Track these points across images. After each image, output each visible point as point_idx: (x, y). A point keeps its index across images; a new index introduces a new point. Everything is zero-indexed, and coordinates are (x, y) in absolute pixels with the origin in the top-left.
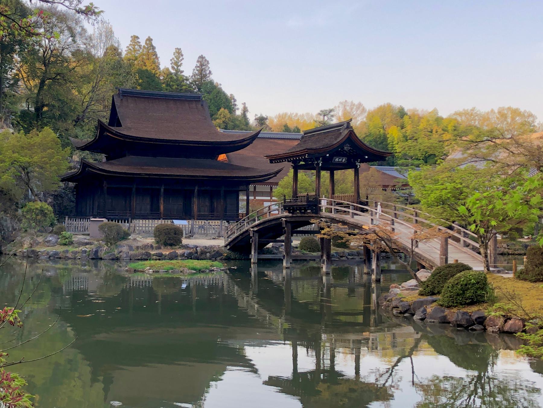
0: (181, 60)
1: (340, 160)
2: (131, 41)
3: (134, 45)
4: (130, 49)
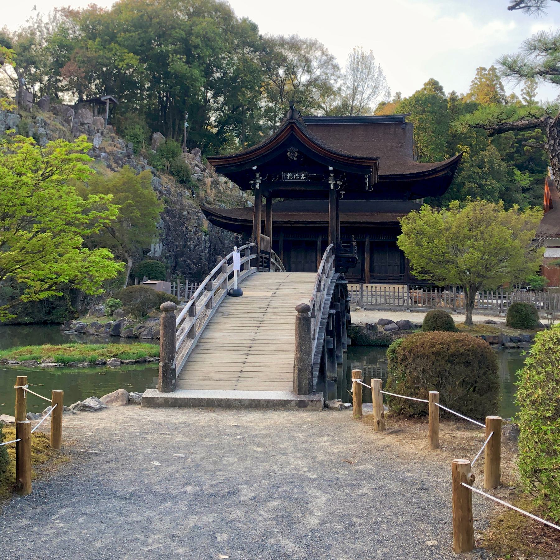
0: (535, 89)
1: (296, 176)
2: (477, 74)
3: (480, 78)
4: (476, 84)
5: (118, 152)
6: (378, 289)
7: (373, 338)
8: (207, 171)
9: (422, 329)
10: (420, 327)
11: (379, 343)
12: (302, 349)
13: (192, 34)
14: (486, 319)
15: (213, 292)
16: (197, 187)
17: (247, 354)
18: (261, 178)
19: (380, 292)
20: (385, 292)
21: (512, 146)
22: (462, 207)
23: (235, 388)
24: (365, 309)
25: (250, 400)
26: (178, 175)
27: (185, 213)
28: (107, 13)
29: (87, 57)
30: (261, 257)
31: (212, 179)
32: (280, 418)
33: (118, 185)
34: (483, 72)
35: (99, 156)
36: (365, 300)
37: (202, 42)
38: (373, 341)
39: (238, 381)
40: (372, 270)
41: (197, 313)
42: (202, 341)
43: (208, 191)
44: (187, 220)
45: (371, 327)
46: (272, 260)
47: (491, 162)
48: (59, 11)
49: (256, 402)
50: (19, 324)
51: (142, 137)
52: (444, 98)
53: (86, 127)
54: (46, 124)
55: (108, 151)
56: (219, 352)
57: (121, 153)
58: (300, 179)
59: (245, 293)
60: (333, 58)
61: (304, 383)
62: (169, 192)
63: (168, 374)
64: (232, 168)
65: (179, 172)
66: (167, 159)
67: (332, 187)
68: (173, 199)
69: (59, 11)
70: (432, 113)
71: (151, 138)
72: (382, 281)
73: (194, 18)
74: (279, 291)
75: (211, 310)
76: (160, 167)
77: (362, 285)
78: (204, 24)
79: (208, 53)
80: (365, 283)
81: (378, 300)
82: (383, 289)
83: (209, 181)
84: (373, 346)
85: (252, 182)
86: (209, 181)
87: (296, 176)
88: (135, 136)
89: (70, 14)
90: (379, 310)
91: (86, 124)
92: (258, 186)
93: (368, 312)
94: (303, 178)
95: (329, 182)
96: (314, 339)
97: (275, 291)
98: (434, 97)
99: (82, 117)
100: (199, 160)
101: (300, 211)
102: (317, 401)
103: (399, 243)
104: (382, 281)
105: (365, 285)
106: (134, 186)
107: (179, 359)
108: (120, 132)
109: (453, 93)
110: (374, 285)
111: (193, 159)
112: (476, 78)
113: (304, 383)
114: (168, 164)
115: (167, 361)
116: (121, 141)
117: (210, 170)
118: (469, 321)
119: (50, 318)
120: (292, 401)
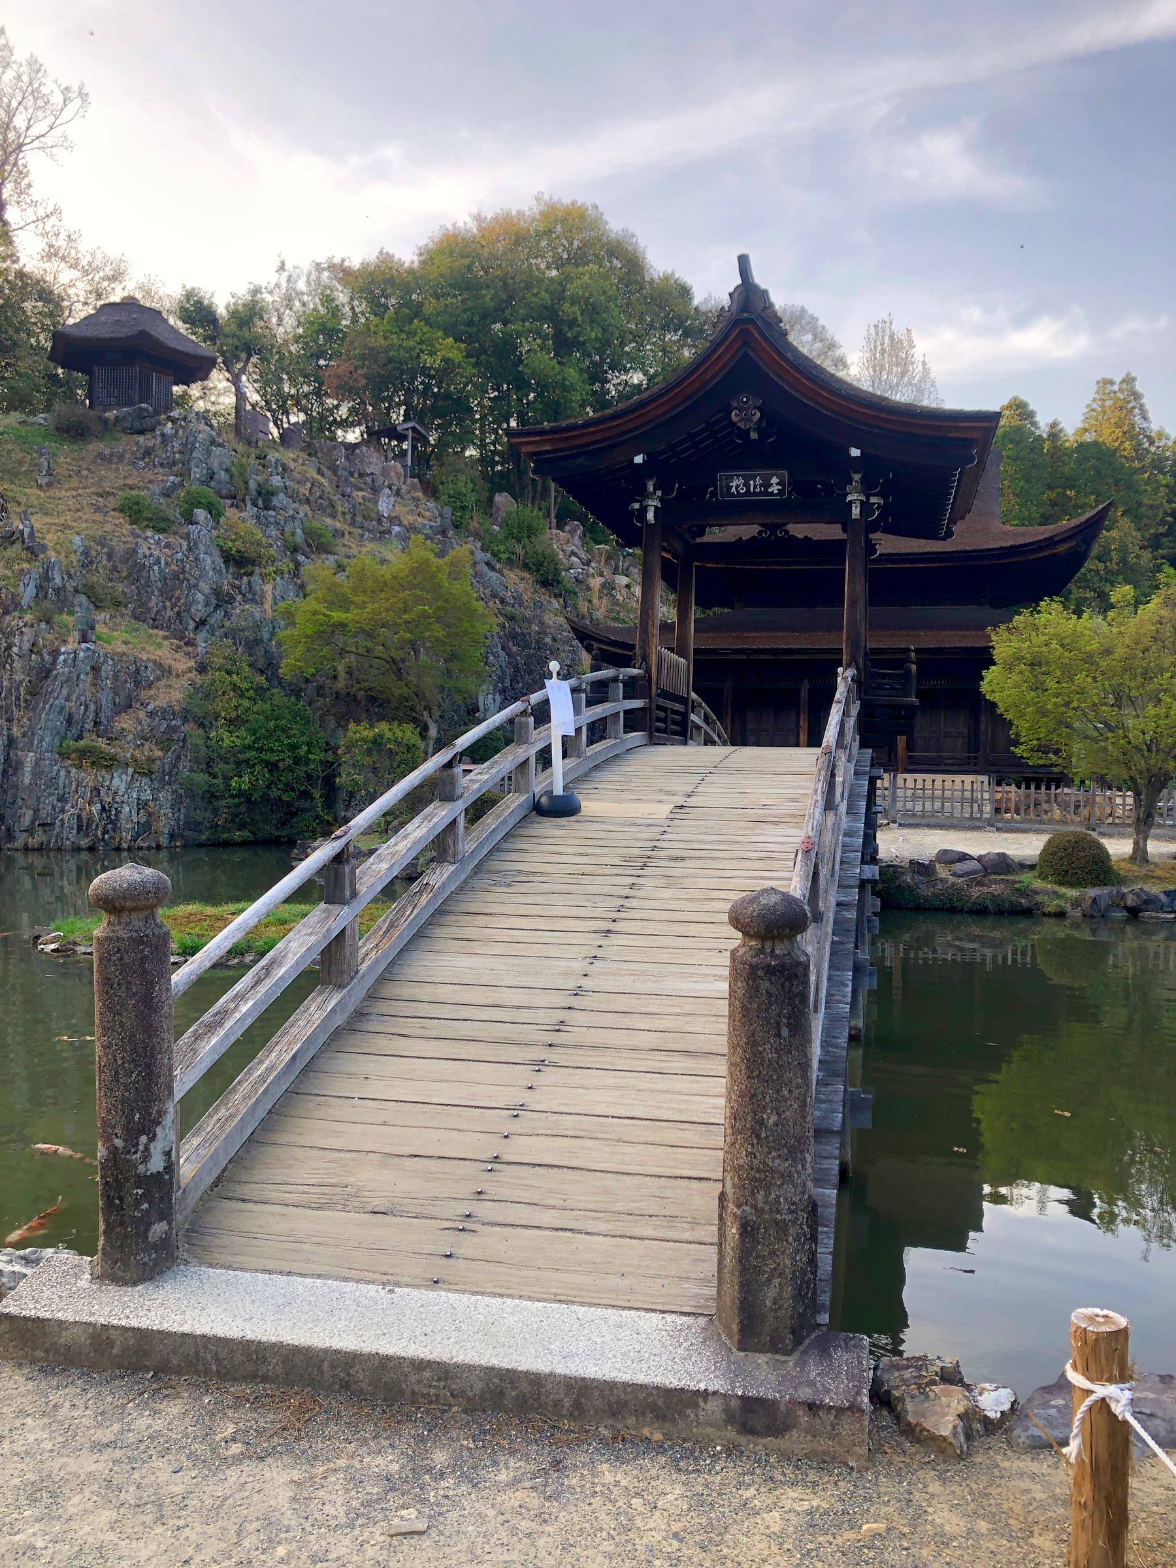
1: (755, 484)
2: (1097, 392)
4: (1093, 410)
5: (424, 525)
6: (929, 784)
7: (926, 891)
8: (593, 564)
9: (1036, 873)
10: (1032, 867)
11: (938, 904)
12: (762, 1123)
13: (564, 299)
15: (460, 806)
16: (575, 594)
17: (540, 1065)
18: (659, 493)
19: (933, 789)
20: (943, 790)
21: (1163, 522)
22: (1139, 601)
23: (441, 1268)
24: (900, 825)
25: (490, 1370)
26: (538, 571)
27: (548, 640)
28: (411, 271)
29: (369, 348)
30: (660, 708)
31: (602, 580)
32: (642, 1502)
33: (401, 575)
34: (1109, 388)
35: (389, 532)
36: (899, 805)
37: (582, 314)
38: (926, 899)
39: (465, 1225)
41: (362, 888)
42: (391, 990)
43: (595, 601)
44: (552, 653)
45: (921, 868)
46: (693, 717)
47: (1123, 550)
48: (323, 269)
49: (525, 1387)
50: (226, 844)
51: (471, 499)
52: (1038, 433)
53: (369, 480)
54: (285, 468)
55: (405, 523)
56: (432, 1048)
57: (431, 527)
58: (766, 493)
59: (589, 806)
60: (834, 346)
61: (772, 1292)
62: (518, 599)
63: (129, 1200)
64: (578, 461)
65: (540, 564)
66: (519, 541)
67: (856, 511)
68: (527, 613)
69: (323, 269)
70: (1015, 460)
71: (490, 500)
72: (932, 768)
73: (569, 269)
74: (692, 801)
75: (452, 868)
76: (504, 556)
77: (895, 776)
78: (584, 279)
79: (593, 334)
80: (896, 770)
81: (928, 806)
82: (938, 784)
83: (596, 582)
84: (925, 909)
85: (637, 506)
86: (596, 582)
87: (755, 484)
88: (457, 496)
89: (343, 273)
90: (929, 826)
91: (368, 475)
92: (650, 516)
93: (905, 831)
94: (775, 489)
95: (849, 498)
96: (816, 1010)
97: (680, 800)
98: (1019, 430)
99: (361, 462)
100: (579, 543)
101: (768, 629)
102: (840, 1410)
103: (984, 687)
104: (932, 768)
105: (901, 777)
106: (433, 577)
107: (245, 1088)
108: (431, 490)
109: (1054, 425)
110: (920, 777)
111: (568, 542)
112: (1094, 400)
113: (772, 1292)
114: (519, 549)
115: (119, 1143)
116: (431, 505)
117: (599, 562)
118: (1140, 855)
119: (282, 833)
120: (705, 1394)
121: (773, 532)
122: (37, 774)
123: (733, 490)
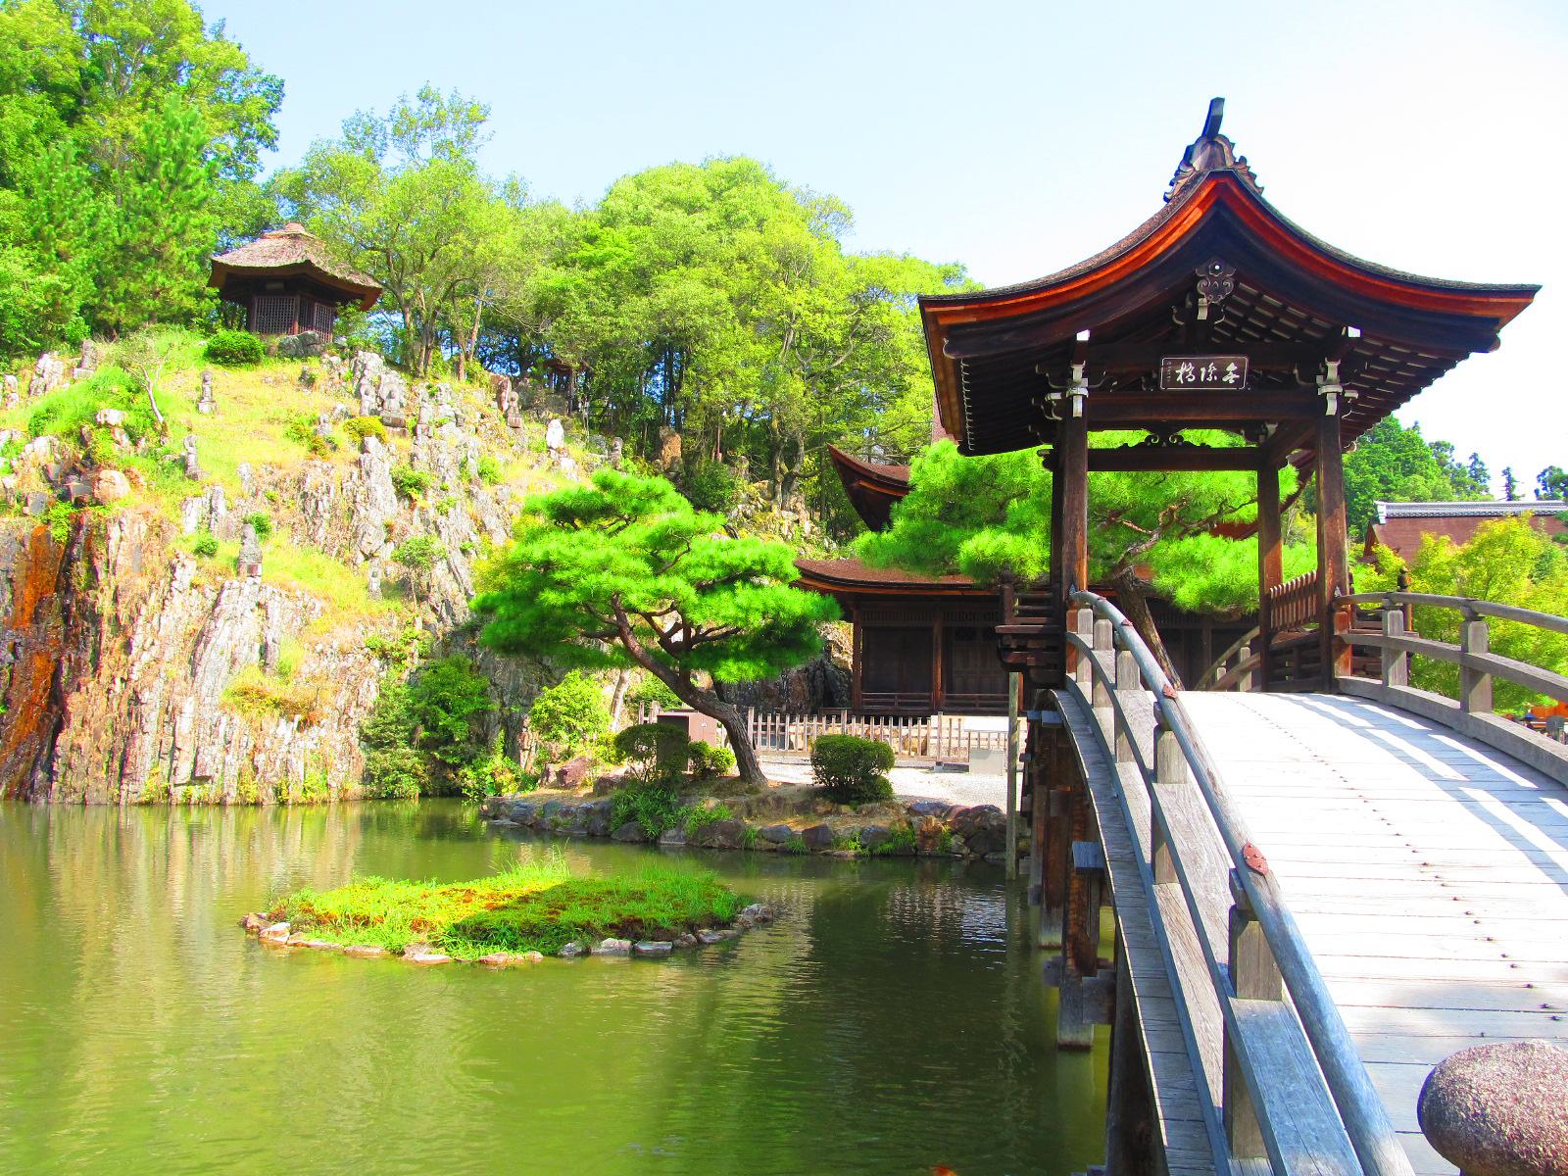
1: (1208, 372)
14: (334, 852)
40: (949, 686)
58: (1220, 383)
67: (1332, 408)
85: (1056, 396)
87: (1208, 372)
94: (1230, 378)
121: (1164, 438)
122: (198, 722)
123: (1180, 378)
